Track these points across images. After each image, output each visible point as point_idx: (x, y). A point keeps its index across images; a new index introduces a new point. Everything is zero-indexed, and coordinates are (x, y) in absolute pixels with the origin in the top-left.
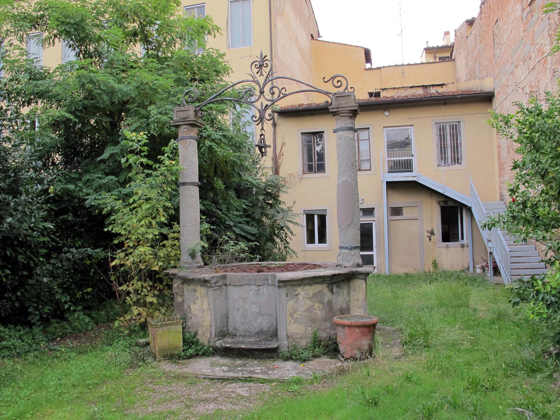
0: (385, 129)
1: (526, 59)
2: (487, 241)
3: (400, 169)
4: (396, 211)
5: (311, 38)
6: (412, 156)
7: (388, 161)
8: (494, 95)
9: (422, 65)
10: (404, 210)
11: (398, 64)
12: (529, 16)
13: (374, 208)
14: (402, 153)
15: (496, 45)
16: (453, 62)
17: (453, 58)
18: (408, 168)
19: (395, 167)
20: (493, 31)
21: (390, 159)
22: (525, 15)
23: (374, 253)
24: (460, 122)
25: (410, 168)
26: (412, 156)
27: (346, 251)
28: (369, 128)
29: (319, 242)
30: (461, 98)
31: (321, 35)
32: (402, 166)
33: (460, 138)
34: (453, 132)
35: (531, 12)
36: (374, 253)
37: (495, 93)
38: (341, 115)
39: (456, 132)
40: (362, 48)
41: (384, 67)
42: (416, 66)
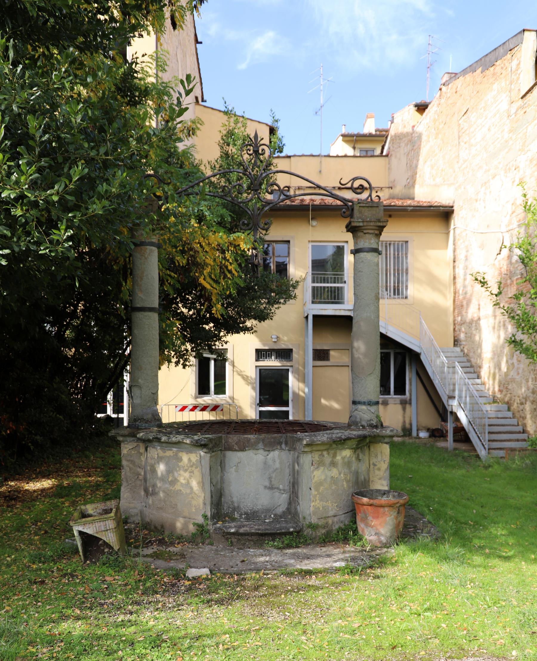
0: (311, 244)
1: (510, 169)
2: (446, 397)
3: (321, 298)
4: (321, 355)
5: (195, 101)
6: (345, 282)
7: (313, 288)
8: (452, 212)
9: (311, 158)
10: (332, 353)
11: (340, 155)
12: (521, 112)
13: (291, 350)
14: (317, 278)
15: (462, 144)
16: (386, 158)
17: (384, 154)
18: (335, 299)
19: (318, 296)
20: (459, 125)
21: (316, 285)
22: (513, 110)
23: (290, 409)
24: (407, 242)
25: (338, 299)
26: (345, 282)
27: (364, 407)
28: (288, 242)
29: (216, 393)
30: (412, 211)
31: (205, 99)
32: (317, 292)
33: (407, 263)
34: (398, 254)
35: (521, 107)
36: (290, 409)
37: (455, 208)
38: (365, 231)
39: (402, 254)
40: (267, 125)
41: (294, 156)
42: (337, 159)
